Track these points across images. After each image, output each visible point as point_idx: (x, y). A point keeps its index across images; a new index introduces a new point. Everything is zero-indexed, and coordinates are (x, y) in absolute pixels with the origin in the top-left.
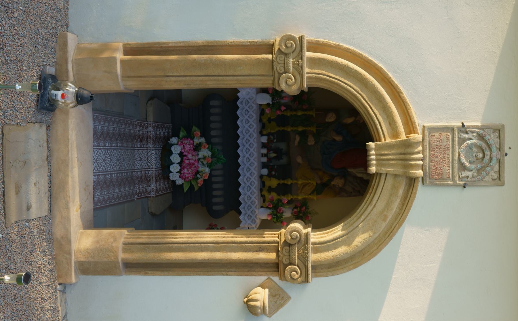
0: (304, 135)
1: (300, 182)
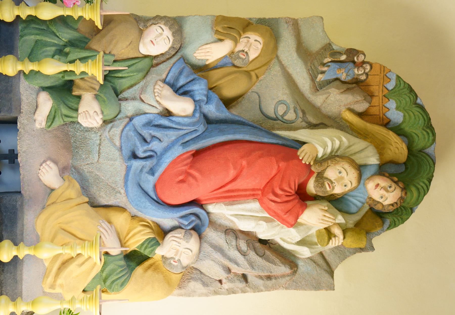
0: (64, 90)
1: (46, 253)
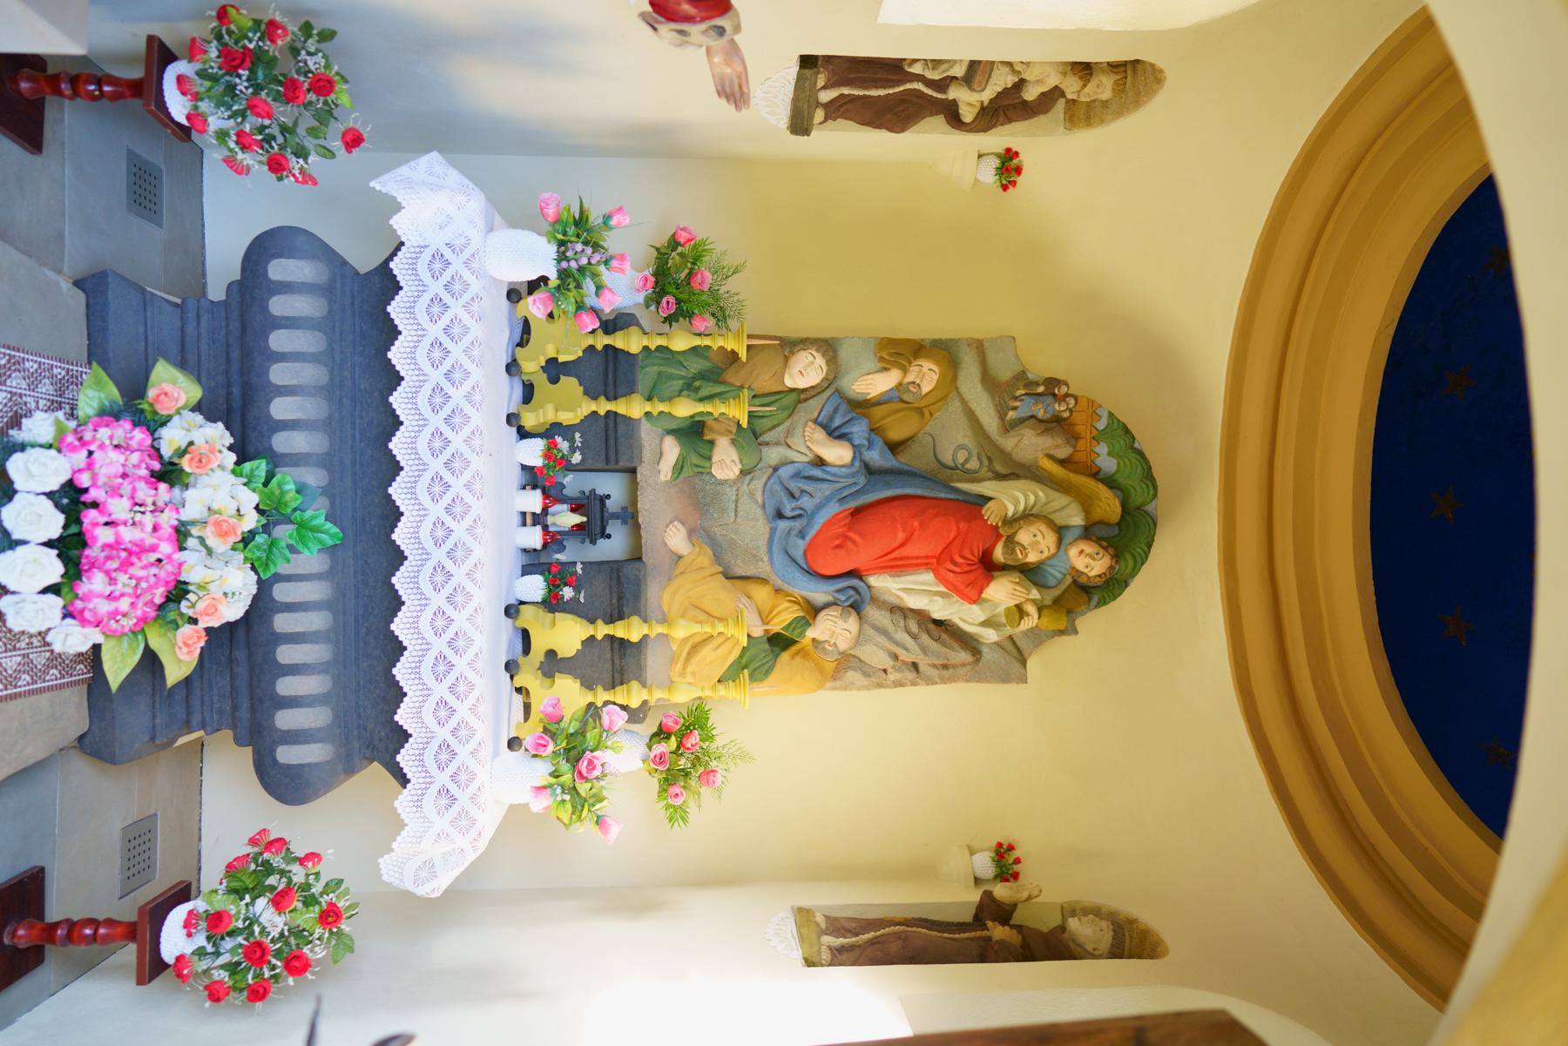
1: (681, 631)
